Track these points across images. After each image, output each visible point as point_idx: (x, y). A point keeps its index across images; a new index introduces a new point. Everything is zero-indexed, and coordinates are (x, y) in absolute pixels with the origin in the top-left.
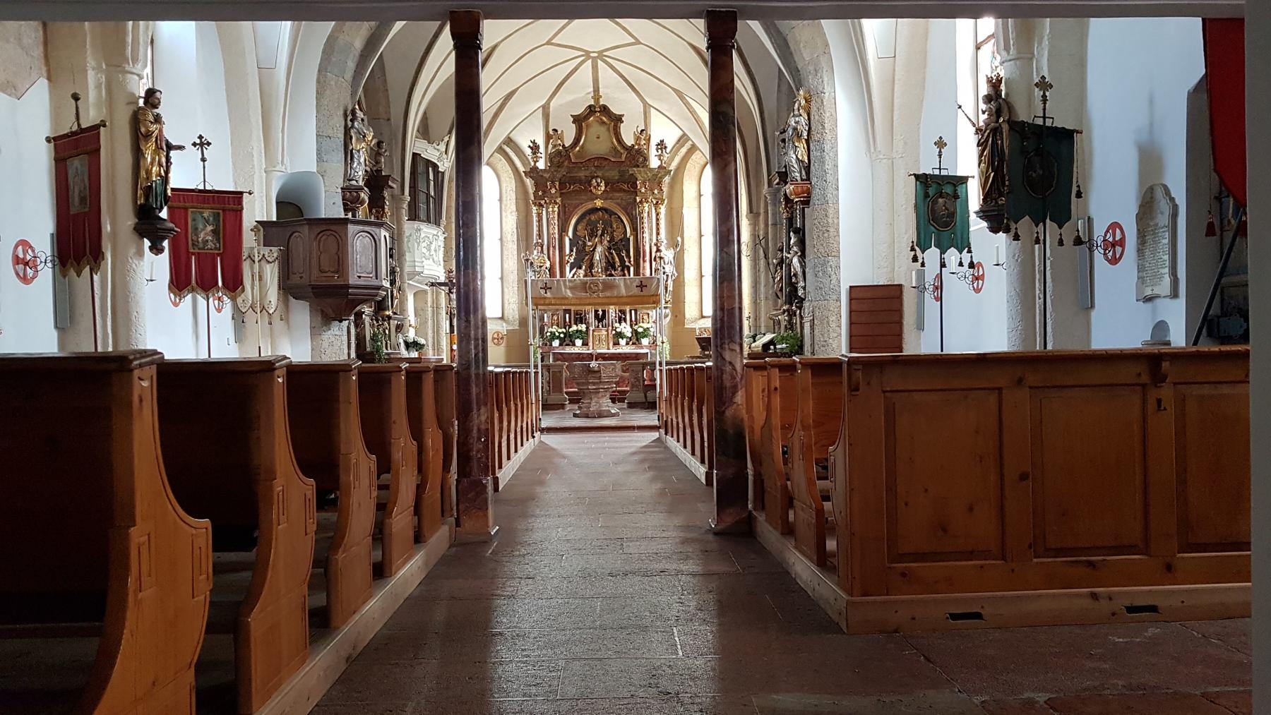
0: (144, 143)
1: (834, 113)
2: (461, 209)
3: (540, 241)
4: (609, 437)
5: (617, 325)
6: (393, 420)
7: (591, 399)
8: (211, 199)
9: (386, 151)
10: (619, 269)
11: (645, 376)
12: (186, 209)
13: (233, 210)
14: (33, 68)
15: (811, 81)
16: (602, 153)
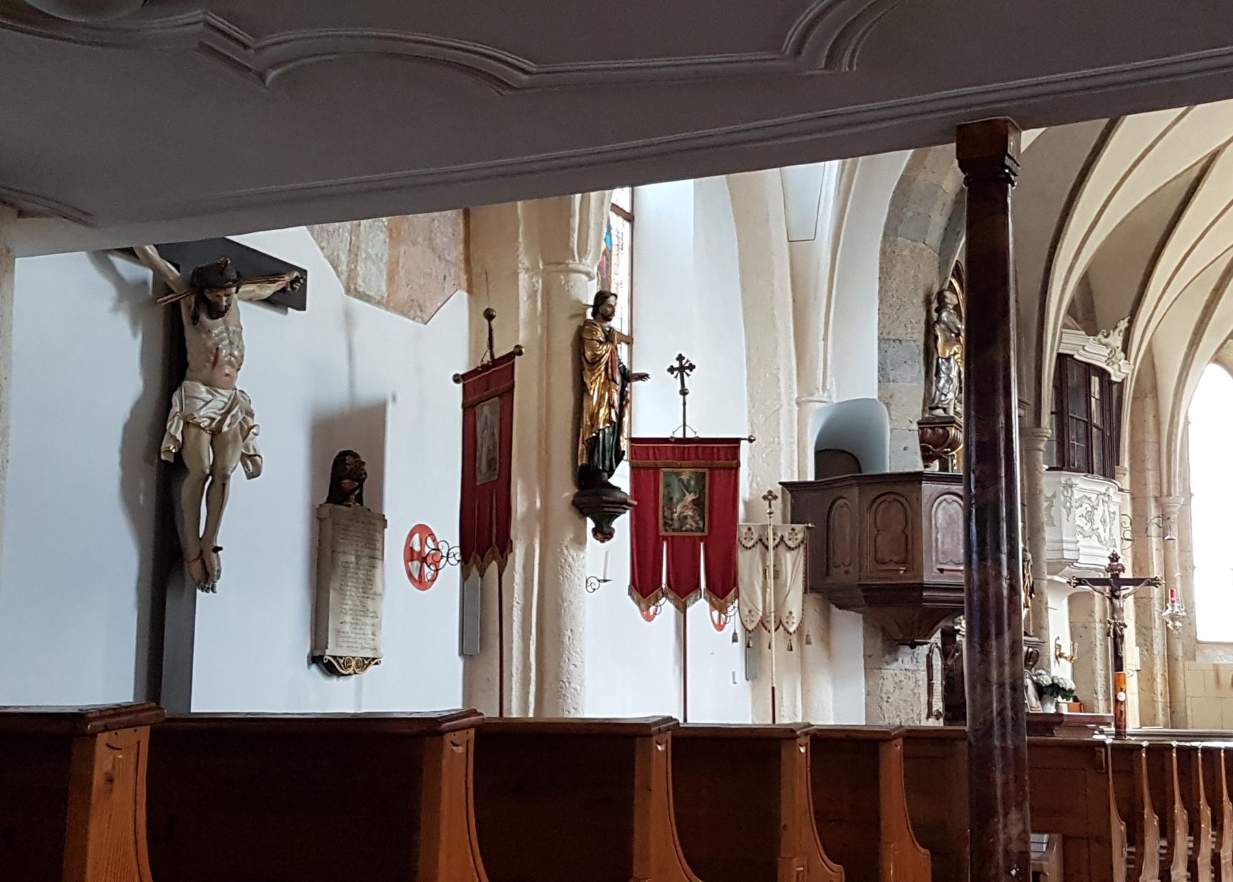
0: (589, 374)
6: (783, 824)
8: (692, 452)
12: (656, 469)
13: (724, 468)
14: (447, 279)
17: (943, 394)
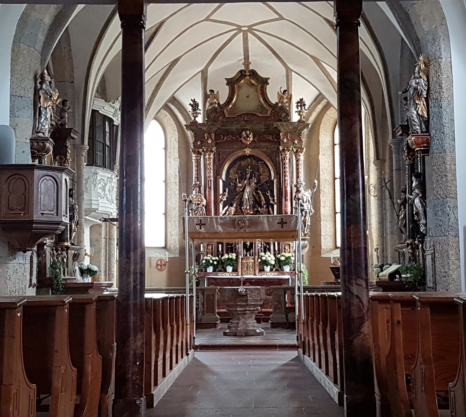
1: (450, 75)
2: (125, 161)
3: (198, 183)
4: (254, 355)
5: (263, 254)
6: (56, 348)
7: (239, 320)
9: (69, 108)
10: (265, 206)
11: (286, 298)
15: (430, 49)
16: (251, 110)
17: (43, 125)
